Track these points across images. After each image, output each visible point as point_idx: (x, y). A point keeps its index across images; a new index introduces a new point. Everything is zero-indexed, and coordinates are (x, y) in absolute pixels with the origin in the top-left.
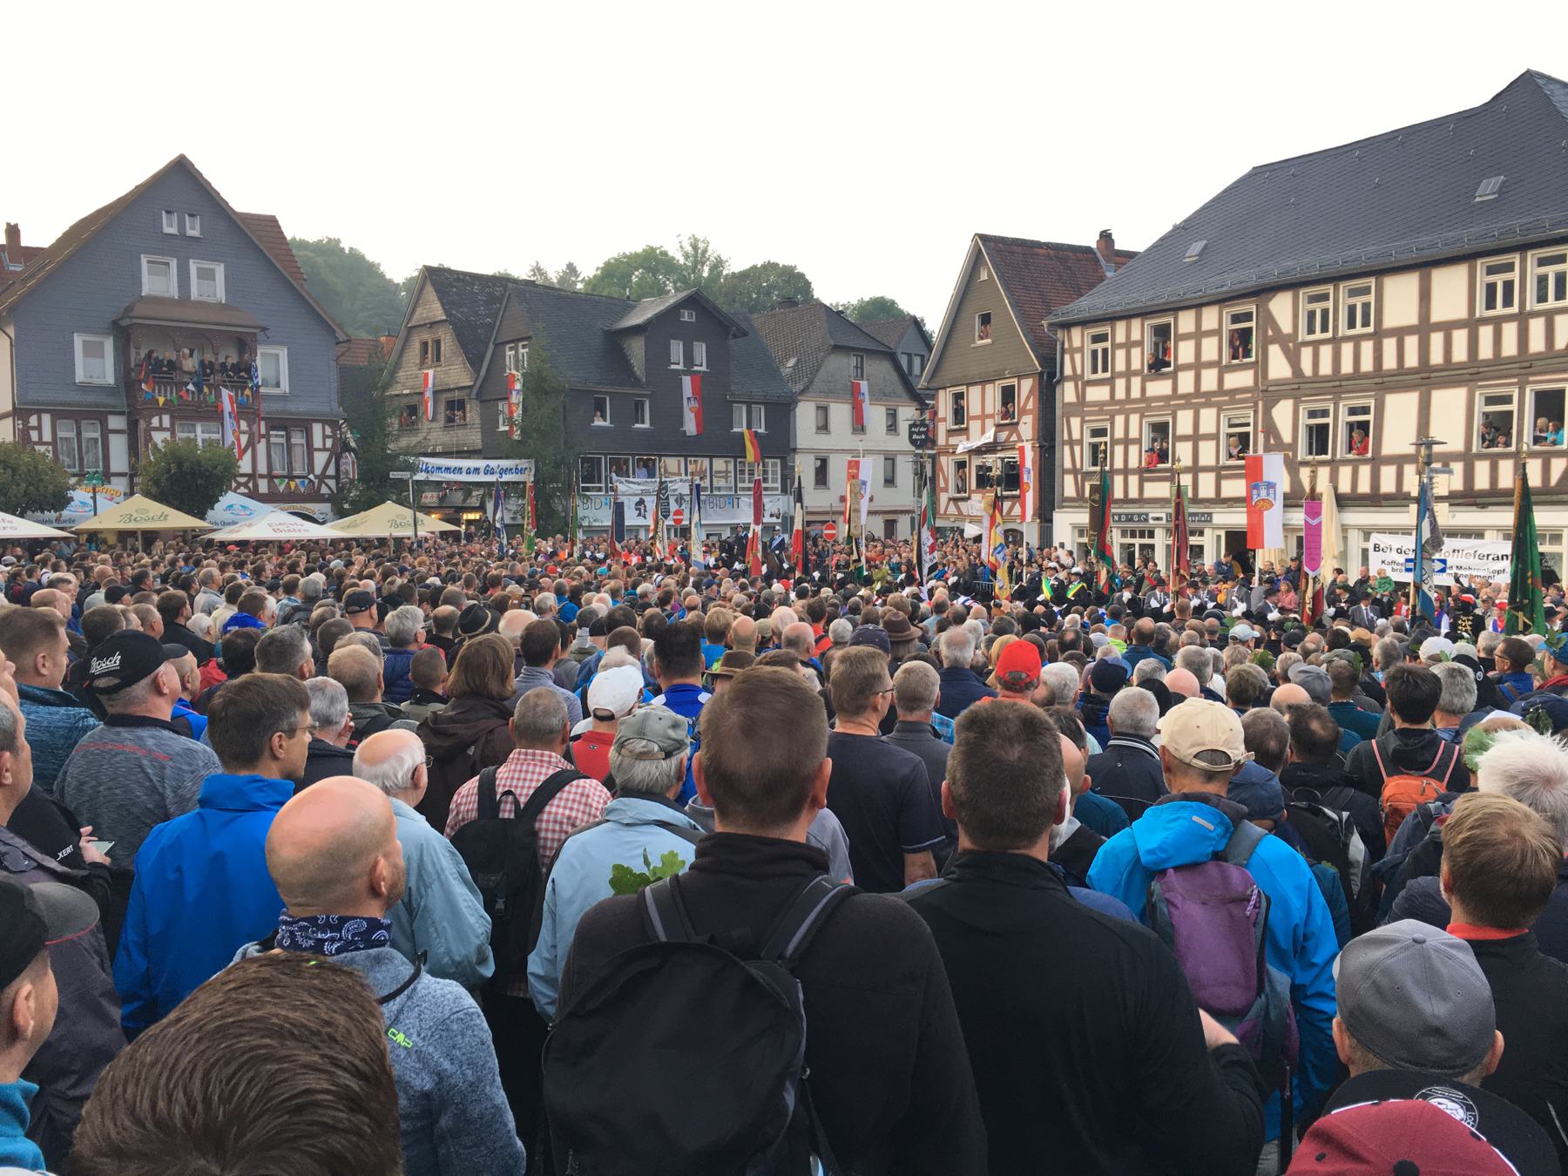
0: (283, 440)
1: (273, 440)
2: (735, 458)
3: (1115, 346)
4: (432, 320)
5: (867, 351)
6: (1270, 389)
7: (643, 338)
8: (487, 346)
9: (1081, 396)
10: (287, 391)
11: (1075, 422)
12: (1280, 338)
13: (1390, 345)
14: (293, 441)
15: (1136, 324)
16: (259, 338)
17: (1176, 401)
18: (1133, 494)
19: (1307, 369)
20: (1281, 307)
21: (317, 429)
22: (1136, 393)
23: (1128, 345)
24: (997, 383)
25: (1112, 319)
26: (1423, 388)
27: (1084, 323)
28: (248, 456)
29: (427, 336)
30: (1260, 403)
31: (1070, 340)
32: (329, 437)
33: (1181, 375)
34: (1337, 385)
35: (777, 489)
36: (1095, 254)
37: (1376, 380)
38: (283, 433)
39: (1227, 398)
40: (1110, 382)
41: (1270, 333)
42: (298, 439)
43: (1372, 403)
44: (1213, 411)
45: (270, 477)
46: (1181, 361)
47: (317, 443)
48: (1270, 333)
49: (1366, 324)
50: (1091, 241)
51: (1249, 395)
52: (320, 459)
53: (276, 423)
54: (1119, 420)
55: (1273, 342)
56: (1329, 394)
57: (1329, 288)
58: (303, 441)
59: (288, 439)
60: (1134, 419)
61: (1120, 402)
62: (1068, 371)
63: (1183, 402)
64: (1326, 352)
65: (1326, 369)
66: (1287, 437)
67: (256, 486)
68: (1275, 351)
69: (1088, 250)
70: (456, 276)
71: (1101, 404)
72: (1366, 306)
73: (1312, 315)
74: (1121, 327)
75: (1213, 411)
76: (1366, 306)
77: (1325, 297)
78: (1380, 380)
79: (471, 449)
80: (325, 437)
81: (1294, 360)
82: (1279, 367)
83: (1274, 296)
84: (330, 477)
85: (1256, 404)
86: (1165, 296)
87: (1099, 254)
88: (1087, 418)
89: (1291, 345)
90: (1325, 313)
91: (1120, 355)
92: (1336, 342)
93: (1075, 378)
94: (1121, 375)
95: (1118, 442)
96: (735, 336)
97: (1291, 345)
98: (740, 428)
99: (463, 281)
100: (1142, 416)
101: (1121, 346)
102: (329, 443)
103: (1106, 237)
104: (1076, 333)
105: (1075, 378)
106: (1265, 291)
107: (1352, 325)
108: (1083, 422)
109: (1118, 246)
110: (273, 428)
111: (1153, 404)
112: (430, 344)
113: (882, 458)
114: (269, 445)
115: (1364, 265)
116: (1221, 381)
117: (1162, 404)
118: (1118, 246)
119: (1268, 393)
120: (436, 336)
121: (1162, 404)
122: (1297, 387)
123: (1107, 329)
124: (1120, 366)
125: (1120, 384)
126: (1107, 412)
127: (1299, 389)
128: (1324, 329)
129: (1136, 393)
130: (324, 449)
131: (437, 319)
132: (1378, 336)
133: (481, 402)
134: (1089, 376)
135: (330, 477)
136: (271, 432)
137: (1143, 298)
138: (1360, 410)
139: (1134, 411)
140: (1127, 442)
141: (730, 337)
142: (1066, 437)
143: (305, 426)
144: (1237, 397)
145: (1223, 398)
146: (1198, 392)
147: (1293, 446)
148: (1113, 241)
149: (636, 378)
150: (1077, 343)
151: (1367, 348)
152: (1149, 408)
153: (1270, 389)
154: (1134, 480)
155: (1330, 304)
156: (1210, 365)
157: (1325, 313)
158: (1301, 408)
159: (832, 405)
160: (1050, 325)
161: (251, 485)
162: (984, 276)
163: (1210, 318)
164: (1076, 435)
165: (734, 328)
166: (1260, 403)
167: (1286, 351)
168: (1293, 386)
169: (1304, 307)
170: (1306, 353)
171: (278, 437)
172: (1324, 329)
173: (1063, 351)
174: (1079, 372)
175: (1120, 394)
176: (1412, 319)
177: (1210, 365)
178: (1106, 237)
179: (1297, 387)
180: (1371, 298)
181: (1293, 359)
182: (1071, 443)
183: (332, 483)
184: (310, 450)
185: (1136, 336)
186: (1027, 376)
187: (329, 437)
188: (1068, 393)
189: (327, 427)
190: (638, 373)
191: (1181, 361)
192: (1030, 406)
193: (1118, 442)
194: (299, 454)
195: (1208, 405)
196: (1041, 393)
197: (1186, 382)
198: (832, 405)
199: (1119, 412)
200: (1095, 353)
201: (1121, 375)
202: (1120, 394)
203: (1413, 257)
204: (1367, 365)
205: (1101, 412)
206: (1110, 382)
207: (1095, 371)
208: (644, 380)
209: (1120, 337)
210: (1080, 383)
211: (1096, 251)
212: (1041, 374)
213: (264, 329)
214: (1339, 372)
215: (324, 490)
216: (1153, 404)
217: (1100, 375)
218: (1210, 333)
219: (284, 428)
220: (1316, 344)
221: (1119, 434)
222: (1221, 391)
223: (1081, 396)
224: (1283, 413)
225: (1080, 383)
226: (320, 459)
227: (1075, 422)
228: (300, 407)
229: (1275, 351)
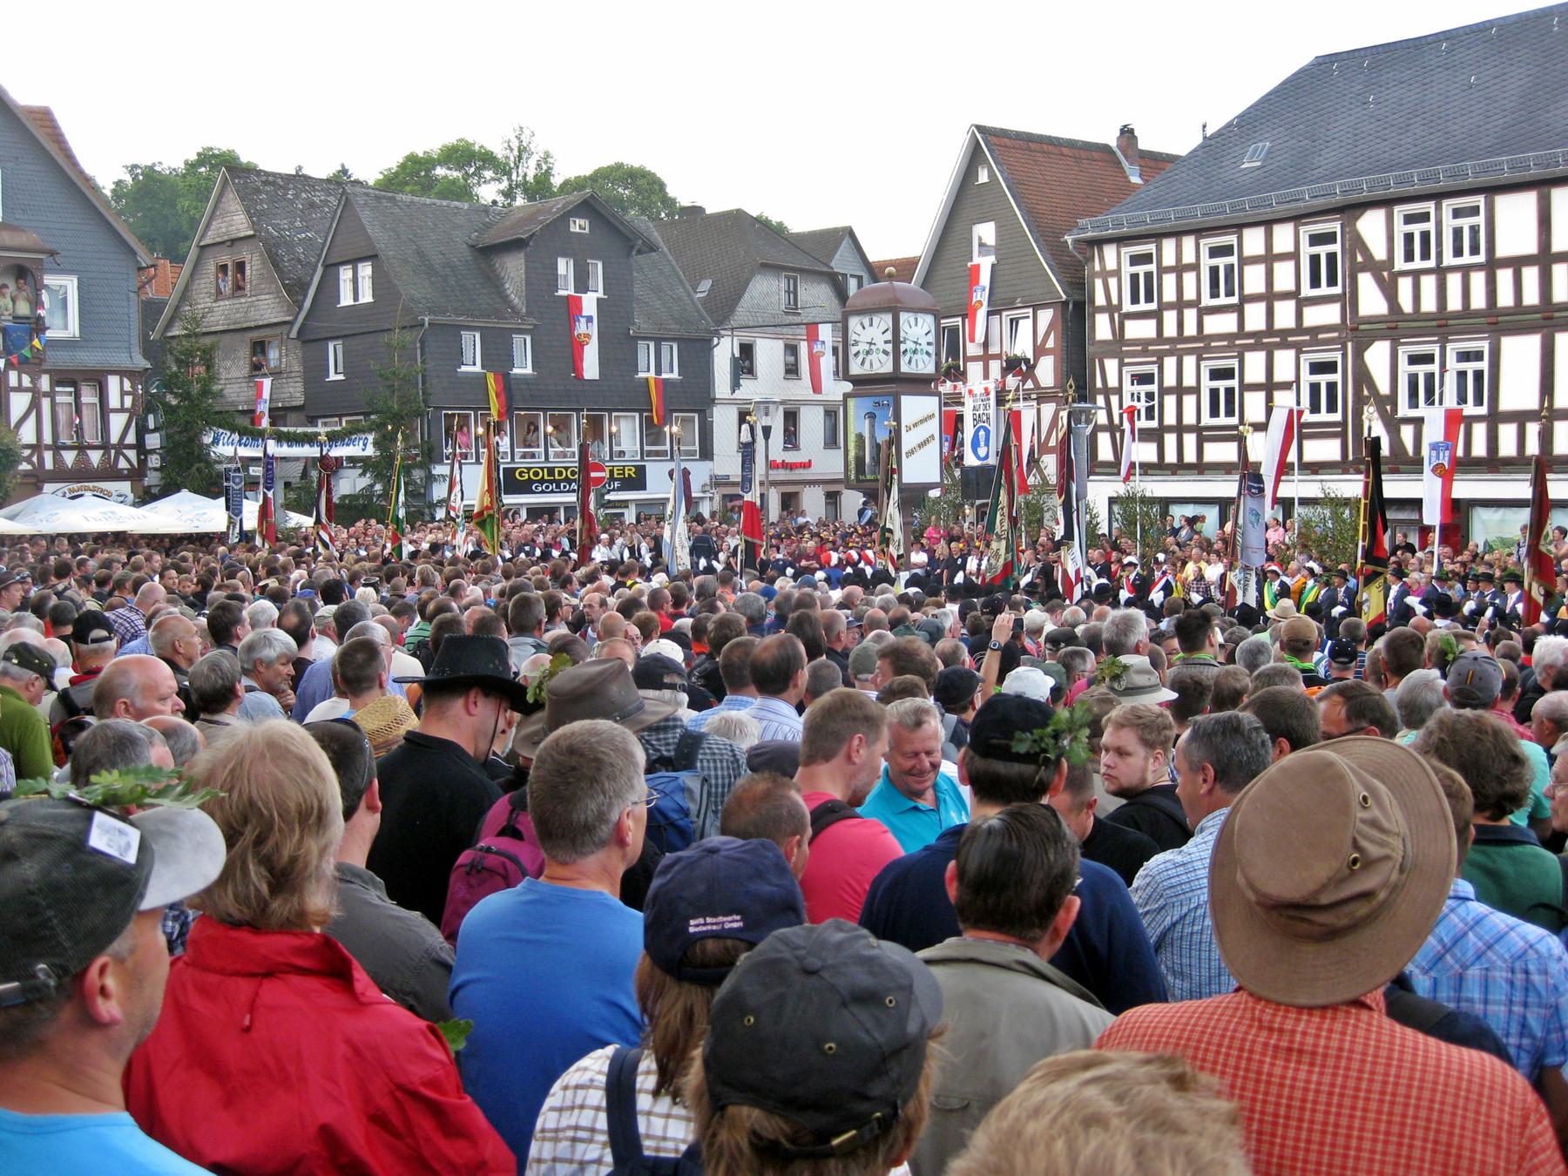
0: (71, 399)
1: (59, 399)
2: (641, 411)
3: (1162, 270)
4: (233, 236)
5: (802, 271)
6: (1362, 327)
7: (522, 255)
8: (315, 271)
9: (1119, 332)
10: (77, 334)
11: (1111, 365)
12: (1372, 266)
13: (1505, 277)
14: (84, 400)
15: (1188, 243)
16: (46, 266)
17: (1241, 341)
18: (1190, 456)
19: (1406, 305)
20: (1371, 225)
21: (113, 383)
22: (1190, 329)
23: (1180, 269)
24: (1004, 314)
25: (1158, 237)
26: (1545, 330)
27: (1121, 240)
28: (31, 423)
29: (226, 258)
30: (1349, 345)
31: (1102, 259)
32: (128, 393)
33: (1248, 308)
34: (1443, 325)
35: (693, 453)
36: (1114, 153)
37: (1490, 320)
38: (72, 389)
39: (1307, 338)
40: (1157, 315)
41: (1360, 259)
42: (89, 397)
43: (1485, 346)
44: (1291, 353)
45: (57, 448)
46: (1248, 290)
47: (114, 402)
48: (1360, 259)
49: (1475, 250)
50: (1111, 138)
51: (1336, 334)
52: (117, 422)
53: (65, 378)
54: (1170, 363)
55: (1363, 269)
56: (1433, 335)
57: (1430, 206)
58: (96, 400)
59: (77, 396)
60: (1189, 362)
61: (1170, 340)
62: (1100, 300)
63: (1252, 341)
64: (1429, 284)
65: (1429, 304)
66: (1384, 388)
67: (41, 460)
68: (1366, 281)
69: (1105, 149)
70: (264, 179)
71: (1145, 343)
72: (1474, 230)
73: (1409, 238)
74: (1169, 246)
75: (1291, 353)
76: (1474, 230)
77: (1425, 217)
78: (1493, 320)
79: (287, 405)
80: (123, 393)
81: (1390, 292)
82: (1371, 302)
83: (1362, 214)
84: (130, 447)
85: (1344, 348)
86: (1226, 210)
87: (1119, 153)
88: (1126, 360)
89: (1385, 274)
90: (1425, 236)
91: (1169, 281)
92: (1441, 272)
93: (1110, 309)
94: (1170, 306)
95: (1170, 391)
96: (639, 252)
97: (1385, 274)
98: (647, 373)
99: (273, 184)
100: (1200, 359)
101: (1169, 270)
102: (128, 401)
103: (1127, 133)
104: (1110, 252)
105: (1110, 309)
106: (1352, 210)
107: (1458, 252)
108: (1121, 365)
109: (1143, 144)
110: (61, 383)
111: (1213, 344)
112: (230, 268)
113: (821, 410)
114: (53, 405)
115: (1471, 181)
116: (1299, 316)
117: (1225, 343)
118: (1143, 144)
119: (1358, 333)
120: (238, 258)
121: (1225, 343)
122: (1395, 327)
123: (1150, 248)
124: (1169, 295)
125: (1170, 318)
126: (1154, 353)
127: (1396, 328)
128: (1425, 255)
129: (1190, 329)
130: (122, 410)
131: (242, 235)
132: (1492, 266)
133: (304, 342)
134: (1128, 307)
135: (130, 447)
136: (58, 389)
137: (1198, 213)
138: (1472, 356)
139: (1189, 352)
140: (1180, 391)
141: (634, 253)
142: (1099, 384)
143: (98, 380)
144: (1320, 336)
145: (1300, 338)
146: (1270, 330)
147: (1393, 398)
148: (1135, 138)
149: (513, 308)
150: (1111, 264)
151: (1478, 280)
152: (1208, 349)
153: (1362, 327)
154: (1190, 440)
155: (1430, 226)
156: (1285, 296)
157: (1425, 236)
158: (1400, 352)
159: (759, 341)
160: (1076, 241)
161: (35, 459)
162: (983, 177)
163: (1283, 237)
164: (1113, 382)
165: (640, 242)
166: (1349, 345)
167: (1380, 281)
168: (1389, 325)
169: (1400, 228)
170: (1405, 285)
171: (64, 397)
172: (1425, 255)
173: (1094, 275)
174: (1115, 301)
175: (1170, 330)
176: (1531, 248)
177: (1285, 296)
178: (1127, 133)
179: (1395, 327)
180: (1480, 220)
181: (1389, 290)
182: (1107, 391)
183: (132, 454)
184: (105, 411)
185: (1189, 257)
186: (1045, 306)
187: (128, 393)
188: (1102, 328)
189: (125, 380)
190: (516, 301)
191: (1248, 290)
192: (1050, 344)
193: (1170, 391)
194: (90, 419)
195: (1284, 345)
196: (1066, 329)
197: (1255, 317)
198: (759, 341)
199: (1170, 353)
200: (1134, 278)
201: (1170, 306)
202: (1170, 330)
203: (1534, 173)
204: (1478, 301)
205: (1145, 353)
206: (1157, 315)
207: (1135, 300)
208: (524, 310)
209: (1169, 259)
210: (1116, 316)
211: (1116, 149)
212: (1065, 303)
213: (52, 253)
214: (1446, 308)
215: (123, 464)
216: (1213, 344)
217: (1143, 306)
218: (1283, 257)
219: (74, 384)
220: (1416, 275)
221: (1170, 380)
222: (1299, 329)
223: (1119, 332)
224: (1377, 357)
225: (1116, 316)
226: (117, 422)
227: (1111, 365)
228: (89, 359)
229: (1366, 281)
